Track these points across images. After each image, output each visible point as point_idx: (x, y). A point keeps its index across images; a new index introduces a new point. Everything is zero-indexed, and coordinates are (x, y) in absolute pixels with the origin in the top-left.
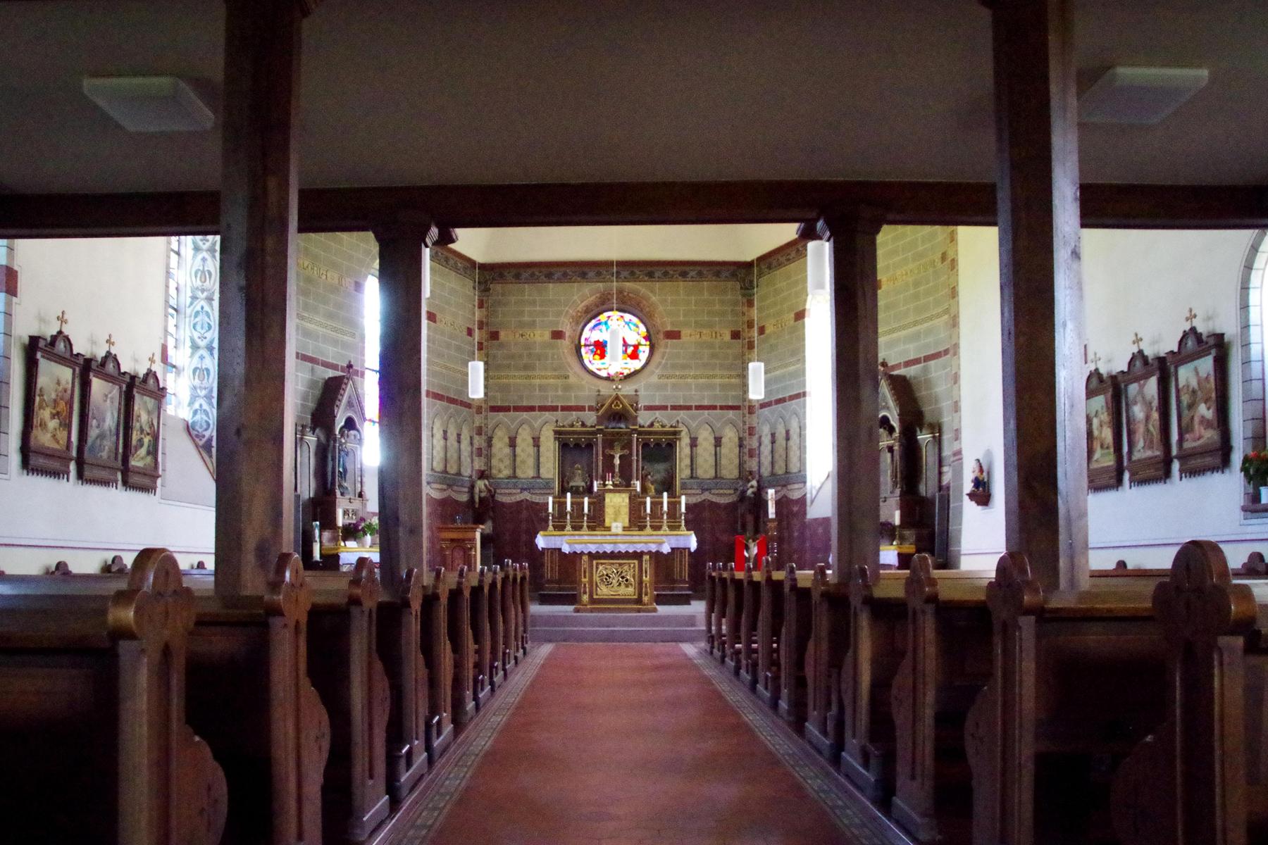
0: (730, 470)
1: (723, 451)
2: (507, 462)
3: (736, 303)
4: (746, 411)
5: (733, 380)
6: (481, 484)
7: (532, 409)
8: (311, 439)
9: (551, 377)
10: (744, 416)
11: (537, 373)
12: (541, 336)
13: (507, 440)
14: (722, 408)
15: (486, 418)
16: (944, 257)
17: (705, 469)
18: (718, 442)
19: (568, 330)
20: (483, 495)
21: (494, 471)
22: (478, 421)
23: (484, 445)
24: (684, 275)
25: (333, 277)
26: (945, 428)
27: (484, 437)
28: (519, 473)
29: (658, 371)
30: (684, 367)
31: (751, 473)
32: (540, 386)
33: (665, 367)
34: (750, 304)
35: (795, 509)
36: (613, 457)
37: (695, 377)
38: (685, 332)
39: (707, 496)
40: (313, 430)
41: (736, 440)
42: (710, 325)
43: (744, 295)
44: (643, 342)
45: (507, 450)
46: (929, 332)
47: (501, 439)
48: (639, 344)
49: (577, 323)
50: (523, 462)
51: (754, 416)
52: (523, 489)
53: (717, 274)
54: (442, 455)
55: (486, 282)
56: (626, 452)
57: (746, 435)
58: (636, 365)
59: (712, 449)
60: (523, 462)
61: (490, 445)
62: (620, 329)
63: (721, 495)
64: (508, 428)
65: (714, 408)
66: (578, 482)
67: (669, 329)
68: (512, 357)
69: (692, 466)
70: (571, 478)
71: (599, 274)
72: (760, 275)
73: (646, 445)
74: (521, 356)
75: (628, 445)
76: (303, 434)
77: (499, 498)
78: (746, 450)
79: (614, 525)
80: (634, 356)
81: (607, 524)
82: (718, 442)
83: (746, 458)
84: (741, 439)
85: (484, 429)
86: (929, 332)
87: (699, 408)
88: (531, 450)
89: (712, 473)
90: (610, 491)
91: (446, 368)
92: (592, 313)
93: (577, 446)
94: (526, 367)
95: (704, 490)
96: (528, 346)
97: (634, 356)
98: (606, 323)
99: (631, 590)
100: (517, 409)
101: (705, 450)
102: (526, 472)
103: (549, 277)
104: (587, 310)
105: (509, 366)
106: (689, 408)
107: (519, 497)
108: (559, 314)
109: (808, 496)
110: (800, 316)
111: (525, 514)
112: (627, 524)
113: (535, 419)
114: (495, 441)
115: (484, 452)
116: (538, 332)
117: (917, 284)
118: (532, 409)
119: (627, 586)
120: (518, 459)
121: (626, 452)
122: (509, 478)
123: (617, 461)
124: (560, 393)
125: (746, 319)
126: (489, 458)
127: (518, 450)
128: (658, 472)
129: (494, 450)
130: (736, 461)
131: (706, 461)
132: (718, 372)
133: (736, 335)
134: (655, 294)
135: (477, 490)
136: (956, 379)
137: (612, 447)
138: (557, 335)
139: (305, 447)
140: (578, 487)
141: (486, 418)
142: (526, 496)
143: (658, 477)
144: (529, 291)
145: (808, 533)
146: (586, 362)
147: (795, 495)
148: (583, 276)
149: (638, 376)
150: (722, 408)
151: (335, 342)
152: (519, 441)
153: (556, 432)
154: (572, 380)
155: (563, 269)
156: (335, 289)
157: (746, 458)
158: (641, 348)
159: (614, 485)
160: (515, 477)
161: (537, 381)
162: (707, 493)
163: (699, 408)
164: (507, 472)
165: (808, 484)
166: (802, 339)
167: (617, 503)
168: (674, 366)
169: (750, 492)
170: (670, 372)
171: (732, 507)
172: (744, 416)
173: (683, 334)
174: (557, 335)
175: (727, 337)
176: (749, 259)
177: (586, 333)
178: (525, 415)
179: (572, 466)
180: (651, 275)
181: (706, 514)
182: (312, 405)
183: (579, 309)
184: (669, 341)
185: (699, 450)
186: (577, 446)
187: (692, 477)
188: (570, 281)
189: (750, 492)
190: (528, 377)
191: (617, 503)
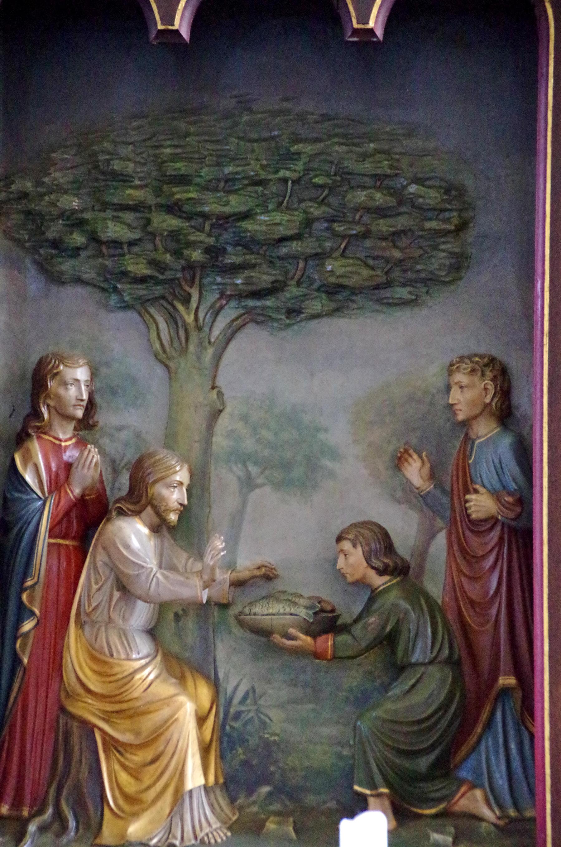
128: (294, 465)
143: (289, 541)
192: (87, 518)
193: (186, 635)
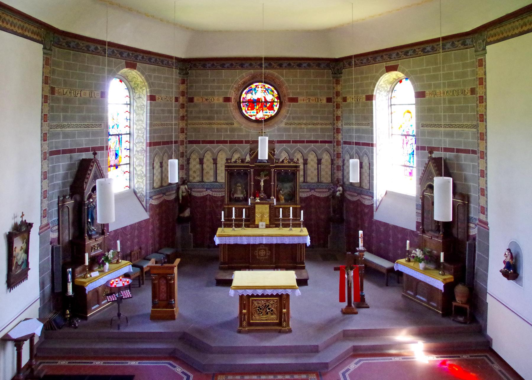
0: (326, 178)
1: (322, 167)
2: (198, 173)
3: (329, 82)
4: (335, 144)
5: (328, 126)
6: (183, 188)
7: (212, 142)
8: (70, 203)
9: (224, 124)
10: (334, 147)
11: (215, 121)
12: (218, 100)
13: (198, 160)
14: (322, 142)
15: (186, 147)
16: (473, 91)
17: (312, 178)
18: (319, 162)
19: (232, 95)
20: (184, 194)
21: (191, 178)
22: (181, 149)
23: (185, 163)
24: (300, 66)
25: (86, 93)
26: (472, 199)
27: (185, 158)
28: (205, 179)
29: (285, 121)
30: (299, 118)
31: (338, 180)
32: (217, 129)
33: (289, 118)
34: (337, 82)
35: (366, 211)
36: (260, 181)
37: (306, 124)
38: (300, 98)
39: (313, 193)
40: (71, 196)
41: (330, 160)
42: (314, 95)
43: (333, 77)
44: (276, 100)
45: (198, 166)
46: (460, 135)
47: (195, 159)
48: (274, 102)
49: (239, 90)
50: (207, 173)
51: (340, 147)
52: (207, 189)
53: (319, 65)
54: (159, 177)
55: (186, 69)
56: (267, 178)
57: (335, 157)
58: (272, 113)
59: (316, 166)
60: (207, 173)
61: (188, 163)
62: (261, 92)
63: (319, 192)
64: (198, 152)
65: (316, 142)
66: (239, 195)
67: (291, 96)
68: (201, 112)
69: (305, 175)
70: (235, 192)
71: (251, 65)
72: (344, 67)
73: (279, 173)
74: (206, 112)
75: (269, 174)
76: (64, 201)
77: (194, 194)
78: (335, 166)
79: (260, 224)
80: (271, 108)
81: (256, 223)
82: (319, 162)
83: (335, 171)
84: (332, 160)
85: (185, 154)
86: (460, 135)
87: (308, 142)
88: (212, 166)
89: (316, 180)
90: (258, 203)
91: (162, 125)
92: (247, 84)
93: (239, 173)
94: (209, 118)
95: (311, 189)
96: (211, 106)
97: (271, 108)
98: (255, 89)
99: (274, 316)
100: (204, 142)
101: (312, 166)
102: (209, 178)
103: (223, 66)
104: (244, 83)
105: (199, 118)
106: (303, 142)
107: (205, 194)
108: (228, 87)
109: (375, 205)
110: (370, 98)
111: (208, 203)
112: (268, 223)
113: (214, 148)
114: (191, 160)
115: (185, 167)
116: (216, 98)
117: (450, 101)
118: (212, 142)
119: (272, 314)
120: (205, 172)
121: (267, 178)
122: (200, 182)
123: (262, 184)
124: (229, 133)
125: (335, 91)
126: (188, 170)
127: (205, 166)
128: (287, 188)
129: (191, 166)
130: (330, 173)
131: (312, 172)
132: (319, 121)
133: (329, 100)
134: (283, 76)
135: (180, 192)
136: (483, 174)
137: (259, 175)
138: (227, 100)
139: (66, 210)
140: (239, 198)
141: (186, 147)
142: (209, 192)
144: (210, 74)
145: (374, 227)
146: (244, 111)
147: (367, 203)
148: (242, 66)
149: (273, 121)
150: (322, 142)
151: (87, 134)
152: (205, 160)
153: (226, 166)
154: (236, 125)
155: (230, 62)
156: (86, 102)
157: (335, 171)
158: (275, 104)
159: (261, 199)
160: (202, 181)
161: (215, 126)
162: (313, 191)
163: (308, 142)
164: (198, 179)
165: (375, 198)
166: (370, 111)
167: (262, 211)
168: (294, 118)
169: (338, 194)
170: (291, 121)
171: (327, 199)
172: (334, 147)
173: (299, 99)
174: (227, 100)
175: (324, 101)
176: (337, 57)
177: (244, 95)
178: (208, 146)
179: (236, 184)
180: (281, 66)
181: (313, 203)
182: (70, 180)
183: (240, 83)
184: (292, 103)
185: (309, 166)
186: (239, 173)
187: (304, 182)
188: (235, 69)
189: (338, 194)
190: (210, 124)
191: (262, 211)
192: (279, 191)
193: (283, 195)
